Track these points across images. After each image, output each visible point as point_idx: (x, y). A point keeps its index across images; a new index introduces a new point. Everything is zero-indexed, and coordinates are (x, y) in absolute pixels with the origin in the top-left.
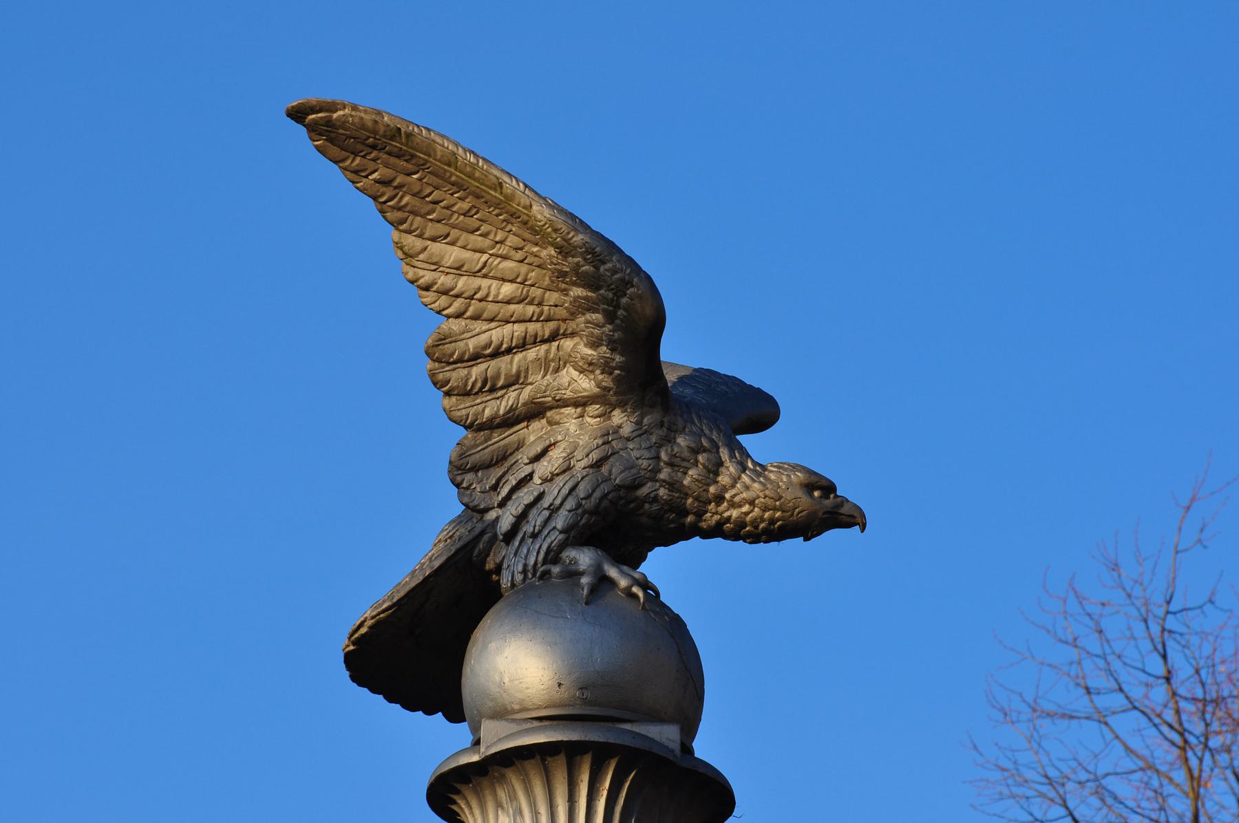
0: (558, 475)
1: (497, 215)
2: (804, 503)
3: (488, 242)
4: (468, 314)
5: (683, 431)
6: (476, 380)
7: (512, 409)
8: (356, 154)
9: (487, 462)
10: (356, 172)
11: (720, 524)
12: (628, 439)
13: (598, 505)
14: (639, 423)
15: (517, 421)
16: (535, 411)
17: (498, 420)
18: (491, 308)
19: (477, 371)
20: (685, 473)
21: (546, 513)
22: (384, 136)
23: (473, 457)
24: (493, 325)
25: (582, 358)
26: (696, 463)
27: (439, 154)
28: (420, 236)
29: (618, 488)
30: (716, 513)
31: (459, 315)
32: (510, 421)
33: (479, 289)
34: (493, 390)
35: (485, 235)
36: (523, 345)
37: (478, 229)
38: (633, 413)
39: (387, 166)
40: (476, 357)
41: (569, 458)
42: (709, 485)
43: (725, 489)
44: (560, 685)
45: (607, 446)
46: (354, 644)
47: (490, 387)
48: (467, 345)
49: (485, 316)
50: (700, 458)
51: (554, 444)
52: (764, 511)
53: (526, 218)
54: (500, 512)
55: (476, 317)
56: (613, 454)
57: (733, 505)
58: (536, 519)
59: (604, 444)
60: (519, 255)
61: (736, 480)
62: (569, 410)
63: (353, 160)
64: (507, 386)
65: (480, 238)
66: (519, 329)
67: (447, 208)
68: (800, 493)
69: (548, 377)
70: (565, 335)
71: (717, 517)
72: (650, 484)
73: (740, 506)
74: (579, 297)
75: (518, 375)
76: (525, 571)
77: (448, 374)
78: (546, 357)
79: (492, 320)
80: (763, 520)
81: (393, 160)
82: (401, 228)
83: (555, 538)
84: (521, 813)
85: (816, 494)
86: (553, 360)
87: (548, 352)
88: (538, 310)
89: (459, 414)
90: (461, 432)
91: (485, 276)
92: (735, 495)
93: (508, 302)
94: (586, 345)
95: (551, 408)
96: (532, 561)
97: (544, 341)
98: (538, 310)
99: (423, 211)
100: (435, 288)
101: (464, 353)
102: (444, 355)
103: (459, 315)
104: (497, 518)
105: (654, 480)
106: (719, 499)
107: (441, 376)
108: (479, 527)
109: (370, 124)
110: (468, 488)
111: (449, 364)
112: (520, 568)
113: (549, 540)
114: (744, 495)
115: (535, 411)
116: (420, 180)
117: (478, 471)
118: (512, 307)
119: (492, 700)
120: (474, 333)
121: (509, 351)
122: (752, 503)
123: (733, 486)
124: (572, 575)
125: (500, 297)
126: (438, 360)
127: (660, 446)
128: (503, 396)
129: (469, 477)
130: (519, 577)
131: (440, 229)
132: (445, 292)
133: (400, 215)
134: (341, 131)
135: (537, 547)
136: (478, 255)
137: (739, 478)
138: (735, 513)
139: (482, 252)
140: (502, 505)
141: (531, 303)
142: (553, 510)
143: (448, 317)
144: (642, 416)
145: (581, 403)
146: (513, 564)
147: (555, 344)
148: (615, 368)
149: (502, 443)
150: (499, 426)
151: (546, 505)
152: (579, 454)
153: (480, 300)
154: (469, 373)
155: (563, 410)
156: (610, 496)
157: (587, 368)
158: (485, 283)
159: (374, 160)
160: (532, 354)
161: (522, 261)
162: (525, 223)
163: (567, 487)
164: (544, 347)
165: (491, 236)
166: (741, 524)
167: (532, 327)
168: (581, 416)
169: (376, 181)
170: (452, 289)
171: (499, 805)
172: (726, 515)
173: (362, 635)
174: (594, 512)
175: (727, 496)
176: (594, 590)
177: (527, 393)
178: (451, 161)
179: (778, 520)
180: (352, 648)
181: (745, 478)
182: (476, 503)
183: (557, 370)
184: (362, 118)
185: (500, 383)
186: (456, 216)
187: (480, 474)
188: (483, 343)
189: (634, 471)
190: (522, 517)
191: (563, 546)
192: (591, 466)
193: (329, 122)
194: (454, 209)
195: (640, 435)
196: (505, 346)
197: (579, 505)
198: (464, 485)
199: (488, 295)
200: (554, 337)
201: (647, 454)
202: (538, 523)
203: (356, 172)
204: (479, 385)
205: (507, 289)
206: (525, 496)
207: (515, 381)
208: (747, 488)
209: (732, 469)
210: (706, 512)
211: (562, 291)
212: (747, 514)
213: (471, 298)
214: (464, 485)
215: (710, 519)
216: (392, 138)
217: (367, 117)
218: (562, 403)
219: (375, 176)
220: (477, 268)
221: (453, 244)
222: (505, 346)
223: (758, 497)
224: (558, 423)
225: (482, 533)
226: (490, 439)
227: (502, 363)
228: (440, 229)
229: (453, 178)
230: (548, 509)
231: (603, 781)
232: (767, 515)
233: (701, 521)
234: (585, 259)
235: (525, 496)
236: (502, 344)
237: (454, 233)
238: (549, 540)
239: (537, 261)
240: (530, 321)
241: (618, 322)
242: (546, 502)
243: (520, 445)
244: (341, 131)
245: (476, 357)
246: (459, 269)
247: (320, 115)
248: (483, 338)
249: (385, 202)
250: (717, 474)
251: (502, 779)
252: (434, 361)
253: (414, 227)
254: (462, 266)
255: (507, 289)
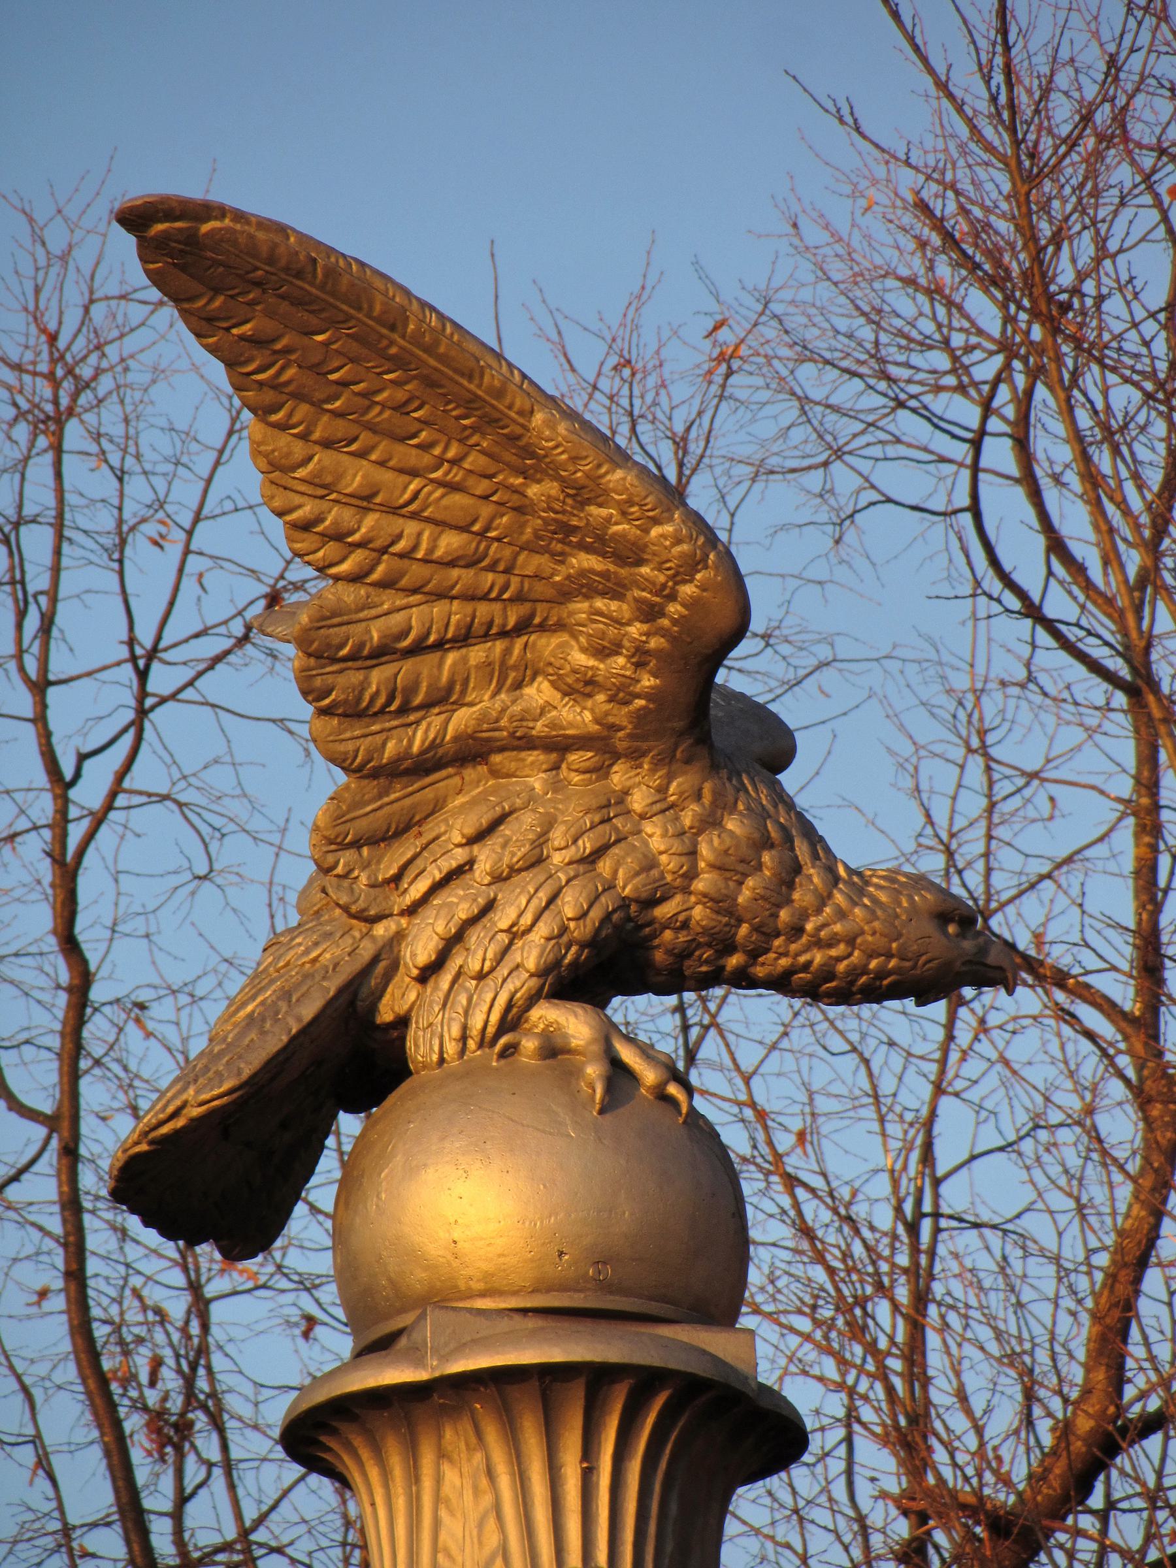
0: (520, 870)
1: (458, 418)
2: (939, 945)
3: (426, 459)
4: (375, 576)
5: (733, 809)
6: (377, 692)
7: (433, 746)
8: (217, 291)
9: (380, 835)
10: (210, 320)
11: (789, 973)
12: (643, 817)
13: (598, 931)
14: (662, 790)
15: (439, 765)
16: (472, 752)
17: (407, 764)
18: (415, 572)
19: (378, 677)
20: (741, 883)
21: (504, 938)
22: (287, 269)
23: (357, 823)
24: (417, 598)
25: (575, 672)
26: (759, 867)
27: (378, 308)
28: (304, 437)
29: (624, 903)
30: (785, 954)
31: (355, 578)
32: (426, 765)
33: (400, 536)
34: (404, 710)
35: (425, 447)
36: (465, 638)
37: (414, 435)
38: (653, 771)
39: (270, 314)
40: (382, 653)
41: (542, 839)
42: (779, 906)
43: (804, 915)
44: (561, 1253)
45: (606, 827)
46: (151, 1143)
47: (403, 706)
48: (368, 631)
49: (403, 583)
50: (766, 857)
51: (510, 813)
52: (871, 956)
53: (518, 430)
54: (404, 922)
55: (386, 584)
56: (618, 841)
57: (818, 943)
58: (477, 953)
59: (602, 822)
60: (483, 487)
61: (823, 900)
62: (532, 756)
63: (211, 300)
64: (427, 706)
65: (414, 451)
66: (458, 613)
67: (363, 395)
68: (929, 927)
69: (503, 696)
70: (543, 628)
71: (784, 962)
72: (678, 898)
73: (830, 945)
74: (592, 571)
75: (450, 689)
76: (464, 1038)
77: (330, 679)
78: (503, 662)
79: (415, 591)
80: (865, 971)
81: (284, 306)
82: (274, 418)
83: (520, 984)
84: (490, 1474)
85: (952, 929)
86: (515, 667)
87: (507, 652)
88: (501, 579)
89: (342, 748)
90: (341, 777)
91: (414, 516)
92: (824, 925)
93: (452, 564)
94: (583, 650)
95: (502, 750)
96: (477, 1022)
97: (503, 634)
98: (501, 579)
99: (318, 396)
100: (319, 529)
101: (362, 645)
102: (329, 646)
103: (355, 578)
104: (400, 936)
105: (686, 891)
106: (797, 931)
107: (318, 682)
108: (367, 951)
109: (264, 250)
110: (345, 876)
111: (334, 660)
112: (456, 1031)
113: (510, 986)
114: (838, 928)
115: (472, 752)
116: (326, 344)
117: (359, 848)
118: (455, 573)
119: (427, 1268)
120: (379, 610)
121: (439, 645)
122: (851, 941)
123: (819, 911)
124: (553, 1049)
125: (439, 553)
126: (318, 656)
127: (698, 834)
128: (418, 722)
129: (345, 859)
130: (451, 1048)
131: (341, 428)
132: (338, 536)
133: (269, 396)
134: (209, 254)
135: (489, 997)
136: (407, 478)
137: (830, 895)
138: (818, 957)
139: (414, 473)
140: (412, 911)
141: (492, 568)
142: (515, 934)
143: (337, 578)
144: (670, 778)
145: (559, 746)
146: (438, 1025)
147: (519, 643)
148: (638, 696)
149: (407, 802)
150: (407, 772)
151: (504, 924)
152: (558, 836)
153: (401, 556)
154: (366, 678)
155: (523, 754)
156: (615, 917)
157: (580, 687)
158: (411, 528)
159: (252, 304)
160: (477, 654)
161: (486, 498)
162: (513, 438)
163: (543, 896)
164: (499, 646)
165: (437, 451)
166: (828, 974)
167: (483, 610)
168: (556, 767)
169: (242, 338)
170: (352, 533)
171: (442, 1455)
172: (802, 959)
173: (177, 1132)
174: (592, 943)
175: (809, 927)
176: (610, 1087)
177: (461, 719)
178: (394, 321)
179: (890, 973)
180: (144, 1147)
181: (839, 898)
182: (361, 904)
183: (518, 685)
184: (251, 237)
185: (417, 701)
186: (377, 409)
187: (365, 851)
188: (395, 630)
189: (655, 873)
190: (454, 941)
191: (533, 1000)
192: (582, 860)
193: (191, 240)
194: (378, 398)
195: (663, 811)
196: (432, 639)
197: (564, 929)
198: (340, 870)
199: (415, 548)
200: (523, 627)
201: (677, 847)
202: (490, 955)
203: (210, 320)
204: (381, 700)
205: (450, 542)
206: (459, 903)
207: (444, 698)
208: (841, 914)
209: (816, 880)
210: (767, 951)
211: (553, 554)
212: (839, 959)
213: (384, 550)
214: (340, 870)
215: (772, 963)
216: (299, 275)
217: (261, 235)
218: (528, 743)
219: (246, 328)
220: (401, 501)
221: (362, 454)
222: (432, 639)
223: (862, 933)
224: (509, 775)
225: (375, 960)
226: (387, 794)
227: (424, 665)
228: (341, 428)
229: (393, 350)
230: (508, 931)
231: (638, 1436)
232: (873, 964)
233: (754, 964)
234: (624, 513)
235: (459, 903)
236: (428, 633)
237: (365, 438)
238: (510, 986)
239: (515, 500)
240: (485, 597)
241: (665, 622)
242: (503, 918)
243: (437, 807)
244: (209, 254)
245: (382, 653)
246: (365, 500)
247: (178, 224)
248: (398, 618)
249: (249, 374)
250: (791, 886)
251: (451, 1412)
252: (310, 655)
253: (294, 420)
254: (375, 494)
255: (450, 542)
